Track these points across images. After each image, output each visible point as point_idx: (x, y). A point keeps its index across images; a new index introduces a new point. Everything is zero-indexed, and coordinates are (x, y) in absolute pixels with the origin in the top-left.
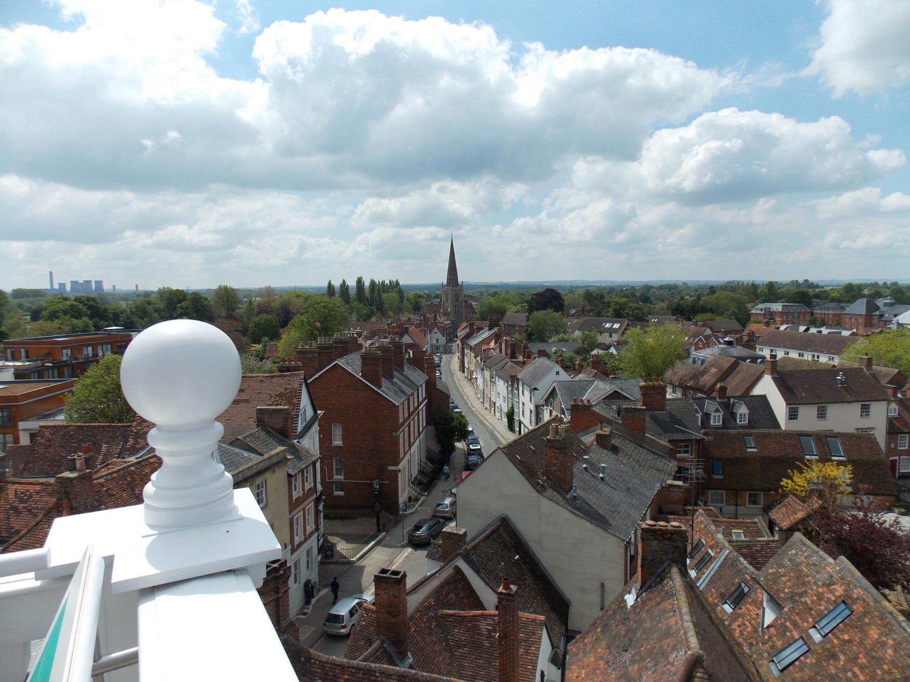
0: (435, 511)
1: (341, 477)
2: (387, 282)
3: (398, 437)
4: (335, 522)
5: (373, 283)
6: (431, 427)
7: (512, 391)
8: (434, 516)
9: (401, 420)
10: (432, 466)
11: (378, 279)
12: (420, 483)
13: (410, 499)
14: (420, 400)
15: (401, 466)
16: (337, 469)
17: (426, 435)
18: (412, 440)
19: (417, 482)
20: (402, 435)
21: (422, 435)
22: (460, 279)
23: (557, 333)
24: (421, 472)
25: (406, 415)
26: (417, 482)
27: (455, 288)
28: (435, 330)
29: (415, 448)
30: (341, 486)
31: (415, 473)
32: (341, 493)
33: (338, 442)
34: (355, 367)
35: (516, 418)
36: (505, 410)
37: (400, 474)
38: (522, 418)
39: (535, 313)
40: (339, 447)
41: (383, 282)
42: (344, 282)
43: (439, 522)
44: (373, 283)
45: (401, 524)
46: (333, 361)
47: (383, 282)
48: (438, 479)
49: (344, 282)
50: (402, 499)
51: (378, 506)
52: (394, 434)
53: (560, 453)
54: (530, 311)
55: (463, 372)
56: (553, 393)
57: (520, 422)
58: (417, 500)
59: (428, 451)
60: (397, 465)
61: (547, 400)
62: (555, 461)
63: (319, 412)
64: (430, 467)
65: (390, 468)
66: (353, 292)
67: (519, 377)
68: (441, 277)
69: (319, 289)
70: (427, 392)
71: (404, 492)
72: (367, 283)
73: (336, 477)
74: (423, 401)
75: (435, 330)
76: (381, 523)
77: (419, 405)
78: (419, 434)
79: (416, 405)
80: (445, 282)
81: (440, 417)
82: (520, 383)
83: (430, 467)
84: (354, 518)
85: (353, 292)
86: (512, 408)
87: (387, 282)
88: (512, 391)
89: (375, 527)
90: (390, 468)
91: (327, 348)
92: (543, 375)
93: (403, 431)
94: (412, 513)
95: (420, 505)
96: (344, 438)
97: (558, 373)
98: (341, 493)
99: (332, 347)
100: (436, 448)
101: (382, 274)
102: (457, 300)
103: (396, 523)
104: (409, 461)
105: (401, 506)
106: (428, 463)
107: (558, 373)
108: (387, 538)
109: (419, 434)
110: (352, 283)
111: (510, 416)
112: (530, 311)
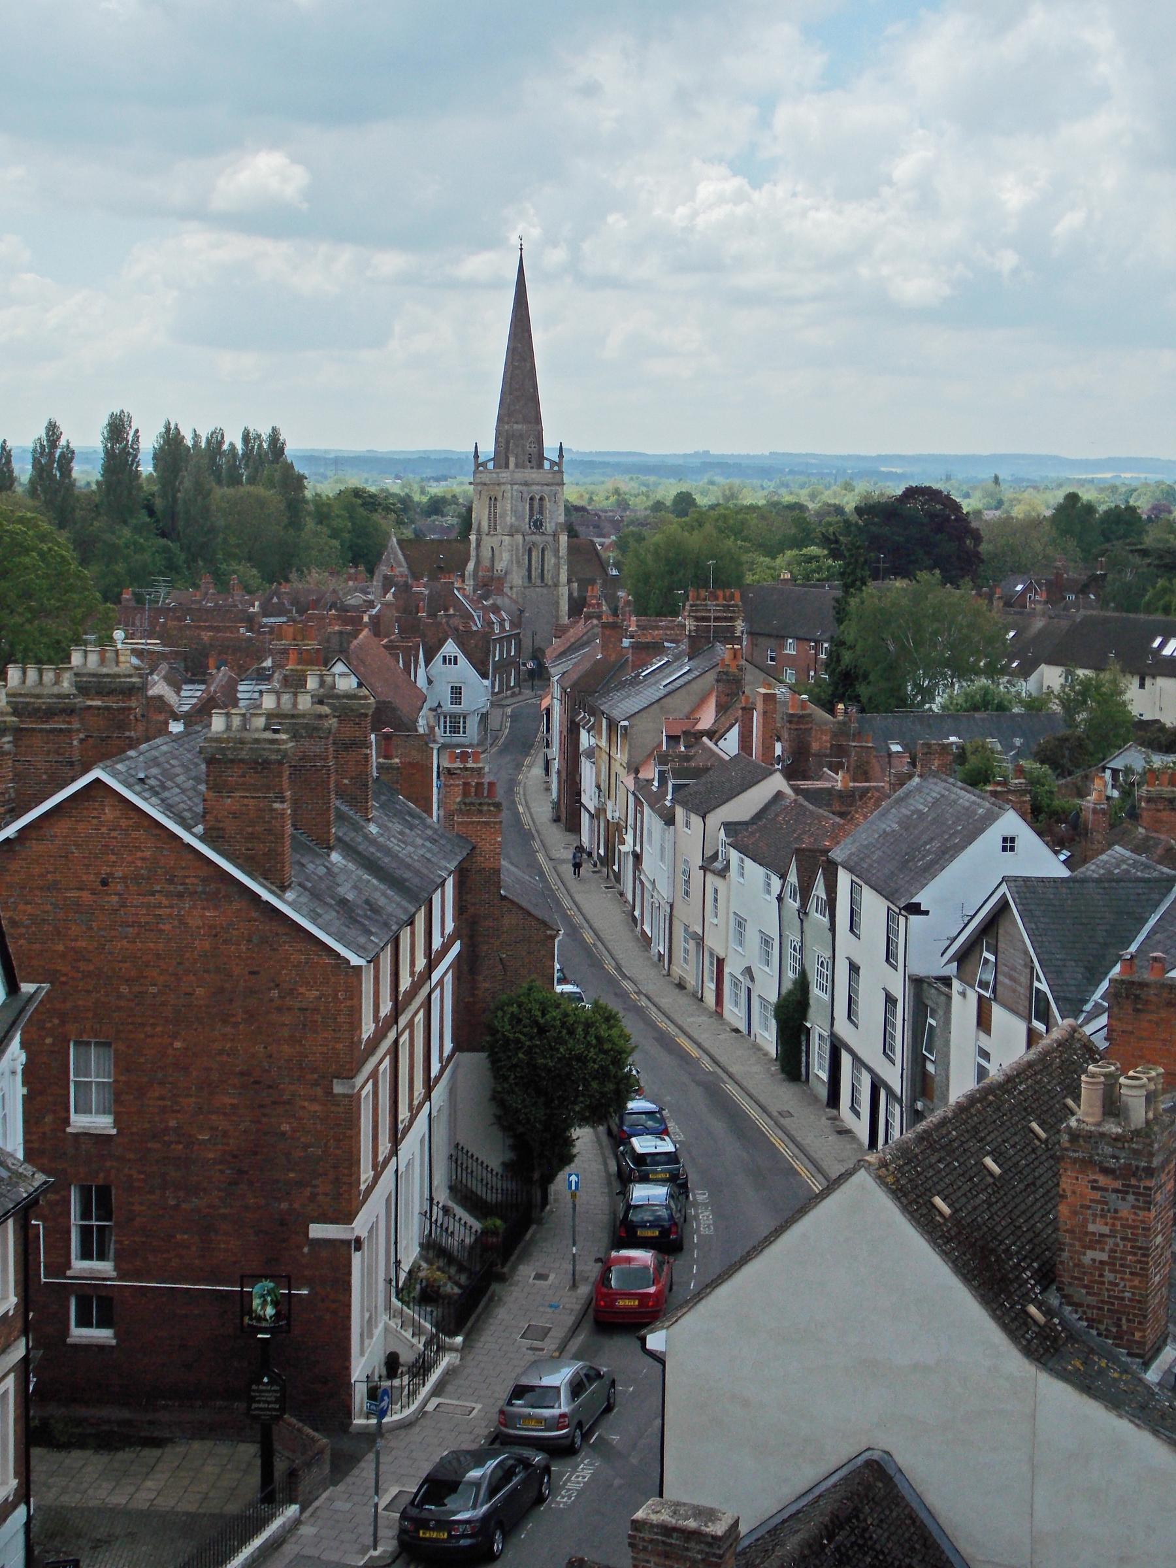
0: (506, 1418)
1: (104, 1267)
2: (233, 438)
3: (353, 1101)
4: (76, 1457)
5: (171, 440)
6: (474, 1060)
7: (803, 912)
8: (499, 1440)
9: (368, 1029)
10: (477, 1225)
11: (195, 427)
12: (428, 1296)
13: (392, 1364)
14: (437, 943)
15: (360, 1226)
16: (86, 1232)
17: (452, 1091)
18: (404, 1114)
19: (418, 1293)
20: (367, 1088)
21: (439, 1093)
22: (553, 436)
23: (963, 671)
24: (431, 1248)
25: (386, 1008)
26: (418, 1293)
27: (532, 475)
28: (450, 648)
29: (411, 1145)
30: (98, 1304)
31: (410, 1254)
32: (102, 1335)
33: (91, 1121)
34: (174, 795)
35: (817, 1025)
36: (769, 990)
37: (356, 1258)
38: (843, 1028)
39: (872, 588)
40: (101, 1140)
41: (216, 440)
42: (53, 431)
43: (526, 1464)
44: (171, 440)
45: (366, 1469)
46: (86, 770)
47: (216, 440)
48: (502, 1278)
49: (53, 431)
50: (363, 1365)
51: (266, 1392)
52: (339, 1088)
53: (1123, 1192)
54: (851, 582)
55: (573, 827)
56: (993, 924)
57: (836, 1047)
58: (422, 1368)
59: (458, 1157)
60: (348, 1218)
61: (964, 957)
62: (1097, 1227)
63: (27, 988)
64: (465, 1227)
65: (317, 1231)
66: (87, 473)
67: (837, 854)
68: (471, 426)
69: (445, 464)
70: (461, 909)
71: (376, 1330)
72: (148, 443)
73: (79, 1265)
74: (446, 948)
75: (450, 648)
76: (280, 1466)
77: (430, 967)
78: (429, 1087)
79: (421, 963)
80: (488, 448)
81: (516, 1020)
82: (844, 879)
83: (465, 1227)
84: (157, 1443)
85: (87, 473)
86: (802, 984)
87: (233, 438)
88: (803, 912)
89: (255, 1479)
90: (317, 1231)
91: (49, 713)
92: (948, 853)
93: (374, 1075)
94: (406, 1425)
95: (437, 1391)
96: (120, 1100)
97: (1009, 844)
98: (102, 1335)
99: (70, 711)
100: (492, 1155)
101: (215, 406)
102: (538, 525)
103: (342, 1466)
104: (393, 1203)
105: (360, 1392)
106: (459, 1211)
107: (1009, 844)
108: (306, 1530)
109: (429, 1087)
110: (86, 440)
111: (792, 1014)
112: (851, 582)
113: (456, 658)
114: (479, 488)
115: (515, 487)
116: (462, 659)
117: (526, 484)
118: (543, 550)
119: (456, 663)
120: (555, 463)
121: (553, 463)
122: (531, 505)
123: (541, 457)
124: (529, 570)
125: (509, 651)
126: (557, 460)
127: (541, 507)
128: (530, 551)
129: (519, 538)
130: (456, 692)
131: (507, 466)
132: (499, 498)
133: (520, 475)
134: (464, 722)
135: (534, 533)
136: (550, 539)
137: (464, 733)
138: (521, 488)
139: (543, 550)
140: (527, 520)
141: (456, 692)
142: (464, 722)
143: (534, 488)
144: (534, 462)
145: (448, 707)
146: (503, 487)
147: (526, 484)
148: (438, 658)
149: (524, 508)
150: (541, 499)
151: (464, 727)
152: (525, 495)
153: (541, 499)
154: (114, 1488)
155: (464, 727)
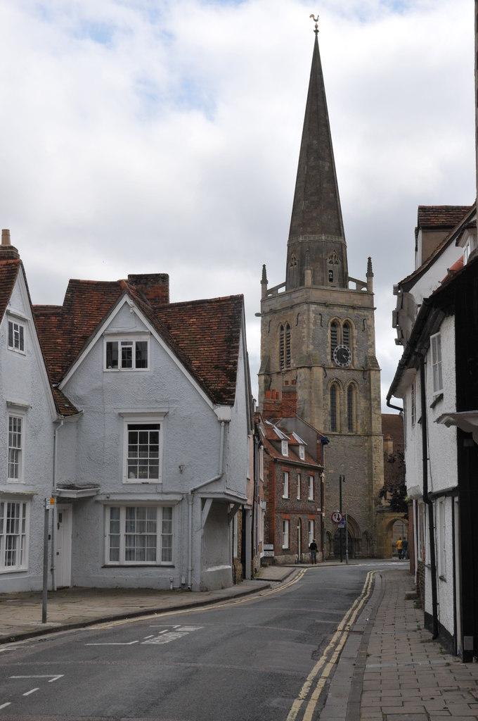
27: (337, 297)
113: (142, 348)
114: (268, 318)
115: (313, 307)
116: (160, 354)
117: (326, 305)
118: (350, 390)
119: (142, 363)
120: (363, 284)
121: (359, 283)
122: (334, 333)
123: (345, 279)
124: (333, 414)
125: (304, 494)
126: (364, 280)
127: (346, 335)
128: (333, 390)
129: (318, 372)
130: (144, 438)
131: (302, 283)
132: (293, 324)
133: (316, 295)
134: (167, 526)
135: (337, 367)
136: (358, 376)
137: (167, 555)
138: (321, 309)
139: (350, 390)
140: (329, 350)
141: (144, 438)
142: (167, 526)
143: (337, 310)
144: (336, 282)
145: (120, 482)
146: (297, 310)
147: (326, 305)
148: (95, 353)
149: (325, 334)
150: (346, 326)
151: (168, 540)
152: (326, 318)
153: (346, 326)
154: (429, 641)
155: (168, 540)
